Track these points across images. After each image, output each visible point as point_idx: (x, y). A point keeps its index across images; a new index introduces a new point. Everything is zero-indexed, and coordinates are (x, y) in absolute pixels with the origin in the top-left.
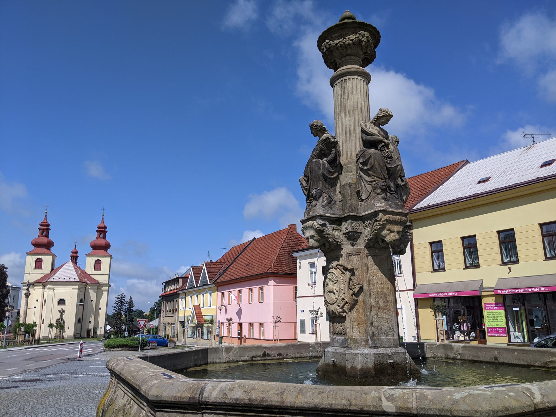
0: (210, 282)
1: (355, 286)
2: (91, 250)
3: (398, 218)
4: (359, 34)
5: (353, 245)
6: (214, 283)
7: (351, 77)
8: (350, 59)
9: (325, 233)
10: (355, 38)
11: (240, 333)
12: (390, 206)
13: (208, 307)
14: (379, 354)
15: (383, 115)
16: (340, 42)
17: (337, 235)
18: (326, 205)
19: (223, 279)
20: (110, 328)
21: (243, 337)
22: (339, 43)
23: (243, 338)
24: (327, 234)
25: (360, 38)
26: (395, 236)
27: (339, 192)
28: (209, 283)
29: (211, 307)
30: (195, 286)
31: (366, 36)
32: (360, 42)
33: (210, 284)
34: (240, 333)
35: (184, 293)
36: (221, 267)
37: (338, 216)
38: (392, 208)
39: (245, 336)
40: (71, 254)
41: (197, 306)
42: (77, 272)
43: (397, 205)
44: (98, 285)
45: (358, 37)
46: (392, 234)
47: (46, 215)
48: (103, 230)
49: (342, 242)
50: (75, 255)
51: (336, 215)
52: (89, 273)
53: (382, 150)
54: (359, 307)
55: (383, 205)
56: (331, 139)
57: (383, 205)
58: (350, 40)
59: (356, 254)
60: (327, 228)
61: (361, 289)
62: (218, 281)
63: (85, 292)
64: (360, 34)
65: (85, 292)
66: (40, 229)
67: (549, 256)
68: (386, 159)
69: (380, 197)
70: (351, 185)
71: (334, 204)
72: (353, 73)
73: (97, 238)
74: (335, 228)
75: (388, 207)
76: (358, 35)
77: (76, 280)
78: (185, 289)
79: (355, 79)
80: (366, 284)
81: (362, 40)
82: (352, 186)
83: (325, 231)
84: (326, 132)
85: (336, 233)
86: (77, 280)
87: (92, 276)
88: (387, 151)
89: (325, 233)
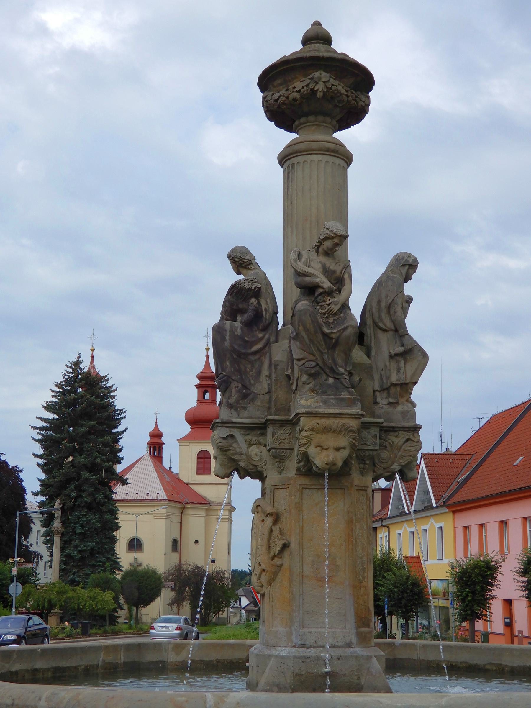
0: (437, 501)
1: (276, 543)
2: (187, 429)
3: (335, 423)
4: (309, 79)
5: (281, 470)
6: (444, 504)
7: (300, 159)
8: (308, 122)
9: (232, 452)
10: (303, 87)
11: (509, 625)
12: (325, 402)
13: (437, 562)
14: (304, 657)
15: (326, 237)
16: (280, 96)
17: (256, 455)
18: (237, 401)
19: (459, 497)
20: (248, 602)
21: (517, 634)
22: (279, 97)
23: (517, 636)
24: (235, 454)
25: (311, 86)
26: (328, 456)
27: (267, 376)
28: (435, 505)
29: (442, 559)
30: (407, 512)
31: (324, 80)
32: (313, 92)
33: (437, 507)
34: (509, 625)
35: (385, 526)
36: (463, 465)
37: (257, 421)
38: (329, 407)
39: (521, 632)
40: (149, 439)
41: (411, 557)
42: (161, 479)
43: (342, 400)
44: (206, 507)
45: (307, 85)
46: (325, 453)
47: (92, 357)
48: (210, 383)
49: (265, 465)
50: (156, 441)
51: (255, 418)
52: (186, 481)
53: (319, 303)
54: (282, 578)
55: (310, 402)
56: (246, 284)
57: (310, 402)
58: (297, 91)
59: (284, 486)
60: (236, 442)
61: (285, 546)
62: (453, 500)
63: (181, 523)
64: (312, 79)
65: (181, 523)
66: (198, 386)
67: (436, 506)
68: (327, 317)
69: (307, 387)
70: (278, 365)
71: (253, 400)
72: (304, 151)
73: (199, 402)
74: (252, 443)
75: (321, 404)
76: (308, 81)
77: (160, 497)
78: (387, 518)
79: (309, 162)
80: (294, 539)
81: (316, 89)
82: (279, 367)
83: (231, 448)
84: (253, 268)
85: (254, 450)
86: (163, 496)
87: (192, 486)
88: (328, 302)
89: (232, 452)
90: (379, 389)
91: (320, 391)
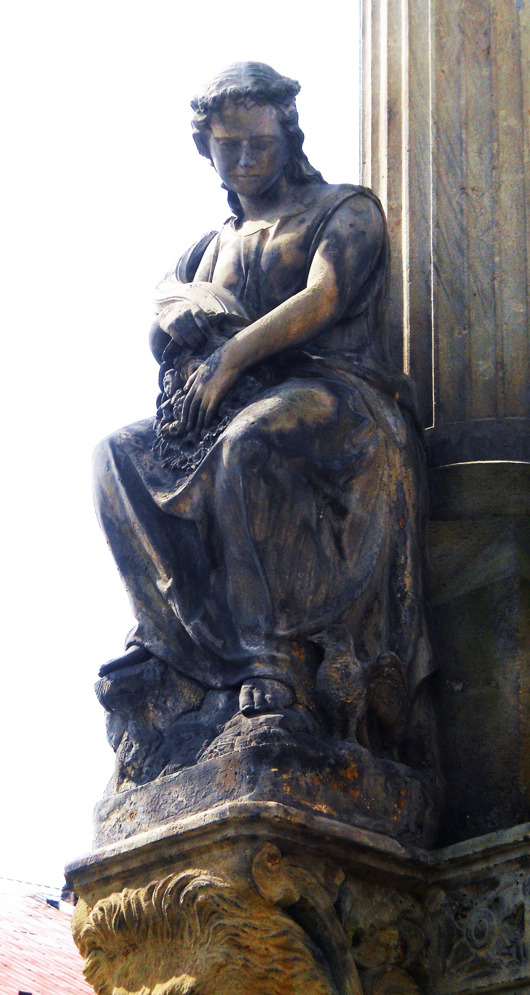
91: (147, 762)
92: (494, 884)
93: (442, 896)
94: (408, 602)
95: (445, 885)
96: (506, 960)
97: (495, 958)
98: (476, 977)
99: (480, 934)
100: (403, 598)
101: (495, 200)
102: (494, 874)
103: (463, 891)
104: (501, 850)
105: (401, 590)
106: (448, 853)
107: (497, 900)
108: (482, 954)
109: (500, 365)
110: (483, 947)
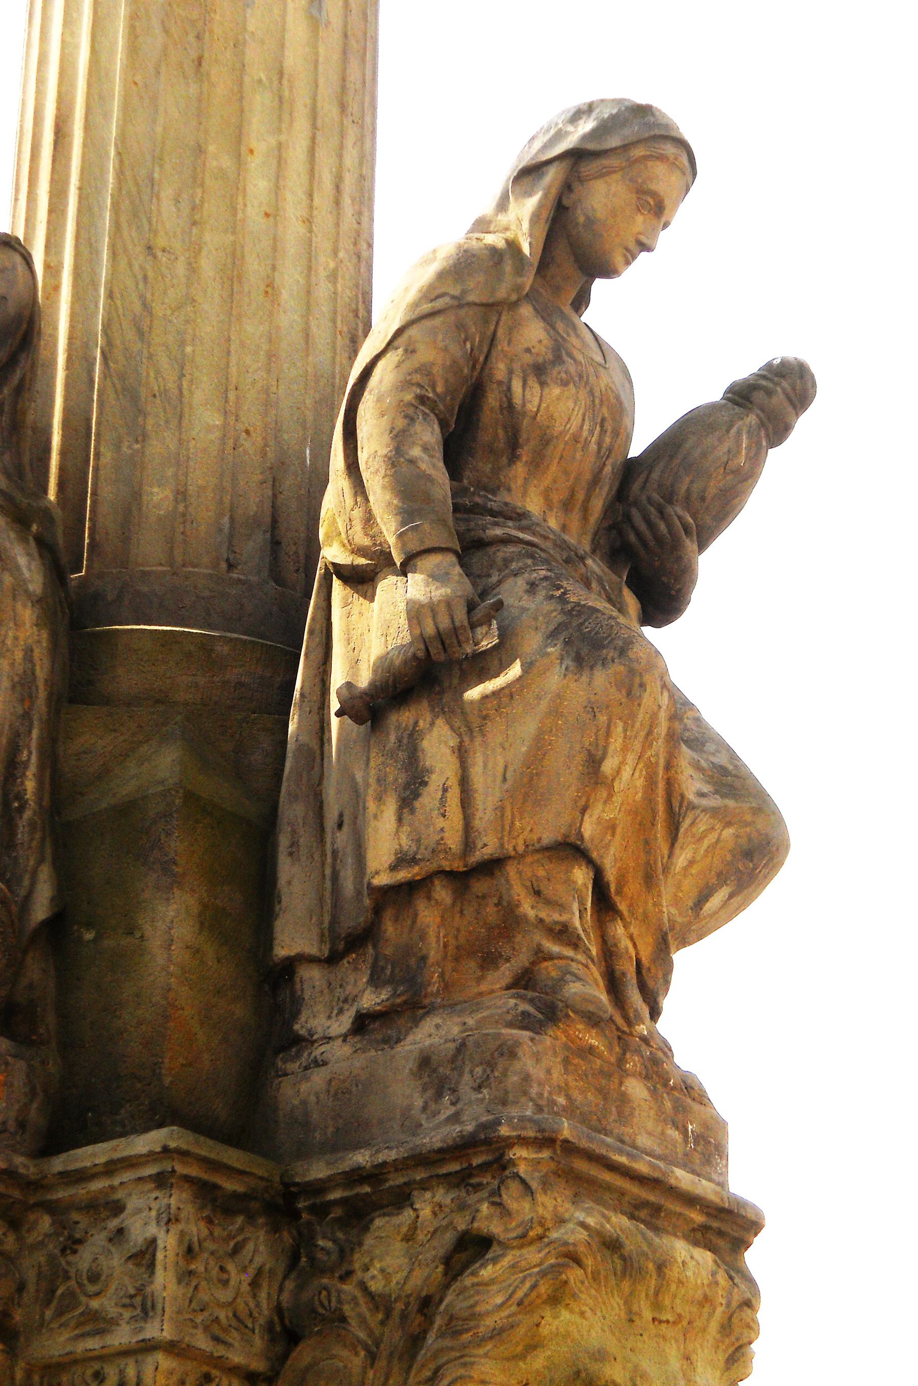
90: (312, 949)
92: (118, 1208)
93: (45, 1223)
94: (28, 814)
95: (51, 1208)
96: (127, 1314)
97: (112, 1310)
98: (82, 1336)
99: (94, 1277)
100: (21, 809)
101: (193, 269)
102: (119, 1195)
103: (75, 1216)
104: (130, 1163)
105: (19, 797)
106: (58, 1164)
107: (120, 1231)
108: (95, 1304)
109: (181, 494)
110: (97, 1294)
